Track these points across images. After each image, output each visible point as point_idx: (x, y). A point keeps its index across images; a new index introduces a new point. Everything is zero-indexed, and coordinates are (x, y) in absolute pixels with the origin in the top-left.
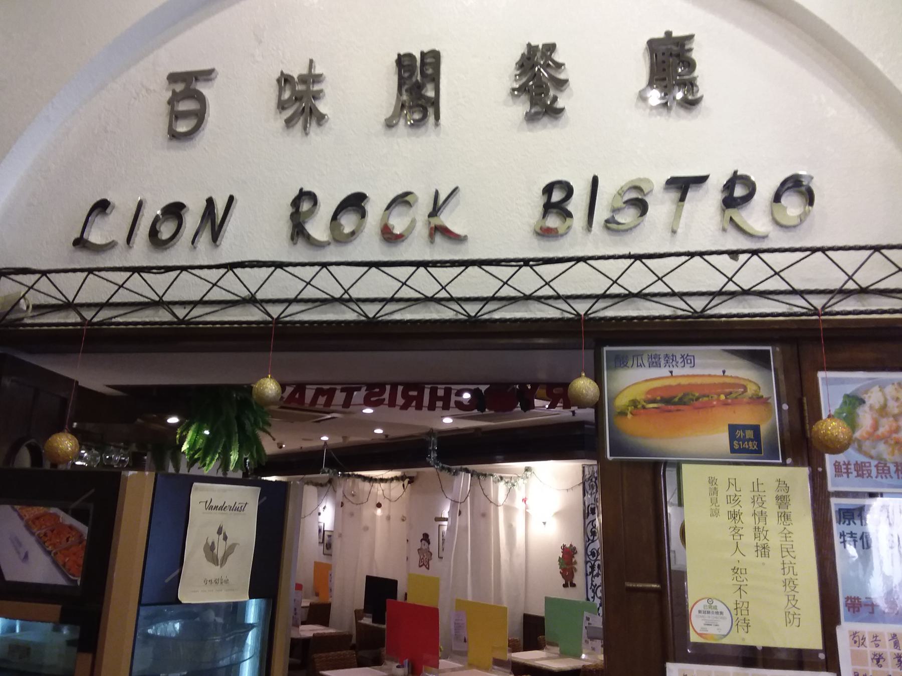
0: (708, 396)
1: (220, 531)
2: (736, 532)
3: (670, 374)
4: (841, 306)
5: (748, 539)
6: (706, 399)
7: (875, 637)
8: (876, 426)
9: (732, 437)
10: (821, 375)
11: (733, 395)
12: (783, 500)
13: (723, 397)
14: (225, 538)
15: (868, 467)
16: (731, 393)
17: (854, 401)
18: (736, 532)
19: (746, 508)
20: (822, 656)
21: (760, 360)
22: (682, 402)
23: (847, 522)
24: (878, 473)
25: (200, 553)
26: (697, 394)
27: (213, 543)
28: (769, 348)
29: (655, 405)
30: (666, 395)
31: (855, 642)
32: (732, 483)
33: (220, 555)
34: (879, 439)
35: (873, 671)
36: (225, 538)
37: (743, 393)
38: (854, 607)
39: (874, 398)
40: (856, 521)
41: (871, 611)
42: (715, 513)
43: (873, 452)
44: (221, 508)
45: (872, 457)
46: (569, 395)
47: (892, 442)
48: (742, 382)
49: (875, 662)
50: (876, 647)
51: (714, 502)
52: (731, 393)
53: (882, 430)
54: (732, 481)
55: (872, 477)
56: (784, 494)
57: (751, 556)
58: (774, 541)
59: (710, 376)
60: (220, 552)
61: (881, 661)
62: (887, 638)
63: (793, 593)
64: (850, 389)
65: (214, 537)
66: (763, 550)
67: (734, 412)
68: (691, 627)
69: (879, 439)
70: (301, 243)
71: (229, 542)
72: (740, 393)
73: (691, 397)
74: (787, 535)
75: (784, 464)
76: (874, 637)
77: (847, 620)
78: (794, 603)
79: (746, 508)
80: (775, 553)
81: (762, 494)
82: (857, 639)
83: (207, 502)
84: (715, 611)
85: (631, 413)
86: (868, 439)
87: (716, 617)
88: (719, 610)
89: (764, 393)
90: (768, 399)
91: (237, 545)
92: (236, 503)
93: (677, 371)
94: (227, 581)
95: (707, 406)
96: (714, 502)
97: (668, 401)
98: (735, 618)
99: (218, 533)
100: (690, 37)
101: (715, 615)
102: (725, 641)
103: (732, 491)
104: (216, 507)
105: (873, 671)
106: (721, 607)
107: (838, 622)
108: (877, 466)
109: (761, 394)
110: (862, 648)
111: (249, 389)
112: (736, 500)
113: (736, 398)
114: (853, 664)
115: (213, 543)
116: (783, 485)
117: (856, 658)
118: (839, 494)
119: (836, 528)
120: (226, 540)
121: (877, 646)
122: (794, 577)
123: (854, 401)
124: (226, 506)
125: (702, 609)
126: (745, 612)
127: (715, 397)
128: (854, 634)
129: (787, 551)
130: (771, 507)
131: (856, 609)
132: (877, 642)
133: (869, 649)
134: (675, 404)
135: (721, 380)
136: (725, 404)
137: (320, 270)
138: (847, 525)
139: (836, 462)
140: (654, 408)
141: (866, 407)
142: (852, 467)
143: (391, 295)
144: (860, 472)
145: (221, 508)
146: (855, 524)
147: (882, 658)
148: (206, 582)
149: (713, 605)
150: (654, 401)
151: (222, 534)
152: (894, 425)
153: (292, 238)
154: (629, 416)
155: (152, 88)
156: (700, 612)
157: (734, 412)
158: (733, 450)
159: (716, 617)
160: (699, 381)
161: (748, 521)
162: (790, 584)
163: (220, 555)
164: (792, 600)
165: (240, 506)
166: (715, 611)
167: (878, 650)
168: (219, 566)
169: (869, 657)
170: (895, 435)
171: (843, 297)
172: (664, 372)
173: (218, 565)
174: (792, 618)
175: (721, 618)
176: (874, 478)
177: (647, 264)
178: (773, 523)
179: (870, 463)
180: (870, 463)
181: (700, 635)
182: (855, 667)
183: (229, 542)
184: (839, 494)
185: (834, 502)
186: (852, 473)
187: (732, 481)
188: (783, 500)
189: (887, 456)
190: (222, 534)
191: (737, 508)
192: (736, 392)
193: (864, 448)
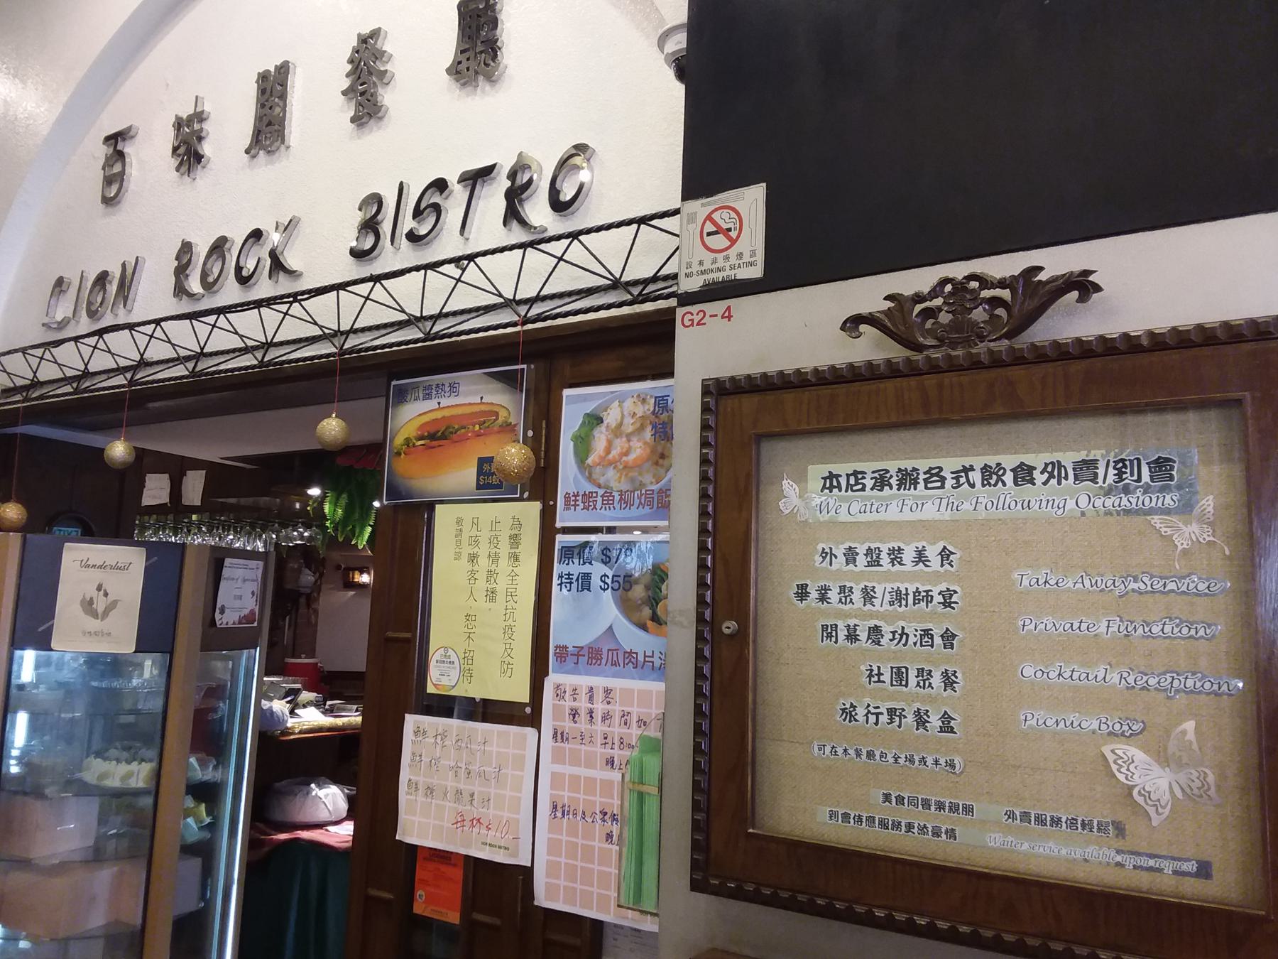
0: (465, 428)
1: (99, 588)
2: (472, 576)
3: (438, 406)
4: (302, 353)
5: (481, 584)
6: (463, 430)
7: (608, 691)
8: (608, 450)
9: (480, 472)
10: (567, 392)
11: (486, 425)
12: (515, 539)
13: (477, 427)
14: (106, 594)
15: (595, 497)
16: (484, 422)
17: (595, 420)
18: (472, 576)
19: (484, 550)
20: (528, 710)
21: (511, 380)
22: (444, 437)
23: (567, 562)
24: (603, 504)
25: (77, 609)
26: (456, 427)
27: (91, 599)
28: (525, 366)
29: (422, 442)
30: (432, 430)
31: (557, 695)
32: (475, 523)
33: (100, 610)
34: (610, 463)
35: (570, 728)
36: (106, 594)
37: (495, 420)
38: (561, 657)
39: (611, 417)
40: (574, 560)
41: (576, 661)
42: (458, 557)
43: (602, 481)
44: (100, 567)
45: (599, 486)
46: (105, 456)
47: (621, 467)
48: (496, 409)
49: (571, 716)
50: (574, 701)
51: (458, 544)
52: (484, 422)
53: (615, 453)
54: (475, 520)
55: (596, 509)
56: (517, 532)
57: (482, 603)
58: (502, 585)
59: (470, 404)
60: (100, 605)
61: (577, 716)
62: (585, 690)
63: (510, 641)
64: (590, 407)
65: (91, 591)
66: (492, 594)
67: (485, 444)
68: (429, 678)
69: (610, 463)
70: (515, 225)
71: (111, 598)
72: (492, 421)
73: (451, 430)
74: (513, 576)
75: (521, 499)
76: (573, 690)
77: (553, 672)
78: (509, 651)
79: (484, 550)
80: (501, 597)
81: (498, 533)
82: (559, 692)
83: (82, 561)
84: (449, 660)
85: (404, 453)
86: (599, 464)
87: (449, 667)
88: (451, 660)
89: (512, 420)
90: (515, 425)
91: (119, 603)
92: (118, 562)
93: (445, 402)
94: (109, 634)
95: (464, 439)
96: (458, 544)
97: (432, 437)
98: (462, 667)
99: (97, 589)
100: (176, 115)
101: (449, 665)
102: (453, 693)
103: (474, 533)
104: (94, 566)
105: (570, 728)
106: (454, 658)
107: (547, 674)
108: (602, 496)
109: (510, 421)
110: (562, 702)
111: (101, 451)
112: (475, 541)
113: (488, 427)
114: (554, 720)
115: (91, 599)
116: (517, 523)
117: (557, 710)
118: (566, 530)
119: (557, 568)
120: (106, 597)
121: (575, 700)
122: (513, 624)
123: (595, 420)
124: (107, 566)
125: (439, 659)
126: (470, 662)
127: (471, 427)
128: (558, 687)
129: (511, 595)
130: (505, 549)
131: (563, 659)
132: (575, 696)
133: (568, 703)
134: (439, 439)
135: (476, 409)
136: (478, 435)
137: (104, 340)
138: (567, 564)
139: (567, 493)
140: (421, 445)
141: (603, 428)
142: (580, 498)
143: (438, 312)
144: (587, 504)
145: (100, 567)
146: (574, 563)
147: (578, 714)
148: (84, 633)
149: (448, 654)
150: (421, 438)
151: (102, 591)
152: (627, 445)
153: (505, 223)
154: (403, 455)
155: (96, 155)
156: (437, 661)
157: (485, 444)
158: (479, 487)
159: (449, 667)
160: (459, 411)
161: (483, 562)
162: (508, 631)
163: (100, 610)
164: (509, 648)
165: (123, 565)
166: (449, 660)
167: (575, 704)
168: (99, 620)
169: (568, 711)
170: (625, 458)
171: (528, 306)
172: (431, 404)
173: (98, 619)
174: (506, 668)
175: (453, 668)
176: (598, 510)
177: (194, 324)
178: (504, 564)
179: (596, 492)
180: (596, 492)
181: (435, 685)
182: (555, 723)
183: (111, 598)
184: (566, 530)
185: (560, 539)
186: (578, 505)
187: (475, 520)
188: (515, 539)
189: (615, 485)
190: (102, 591)
191: (476, 550)
192: (489, 420)
193: (594, 476)
